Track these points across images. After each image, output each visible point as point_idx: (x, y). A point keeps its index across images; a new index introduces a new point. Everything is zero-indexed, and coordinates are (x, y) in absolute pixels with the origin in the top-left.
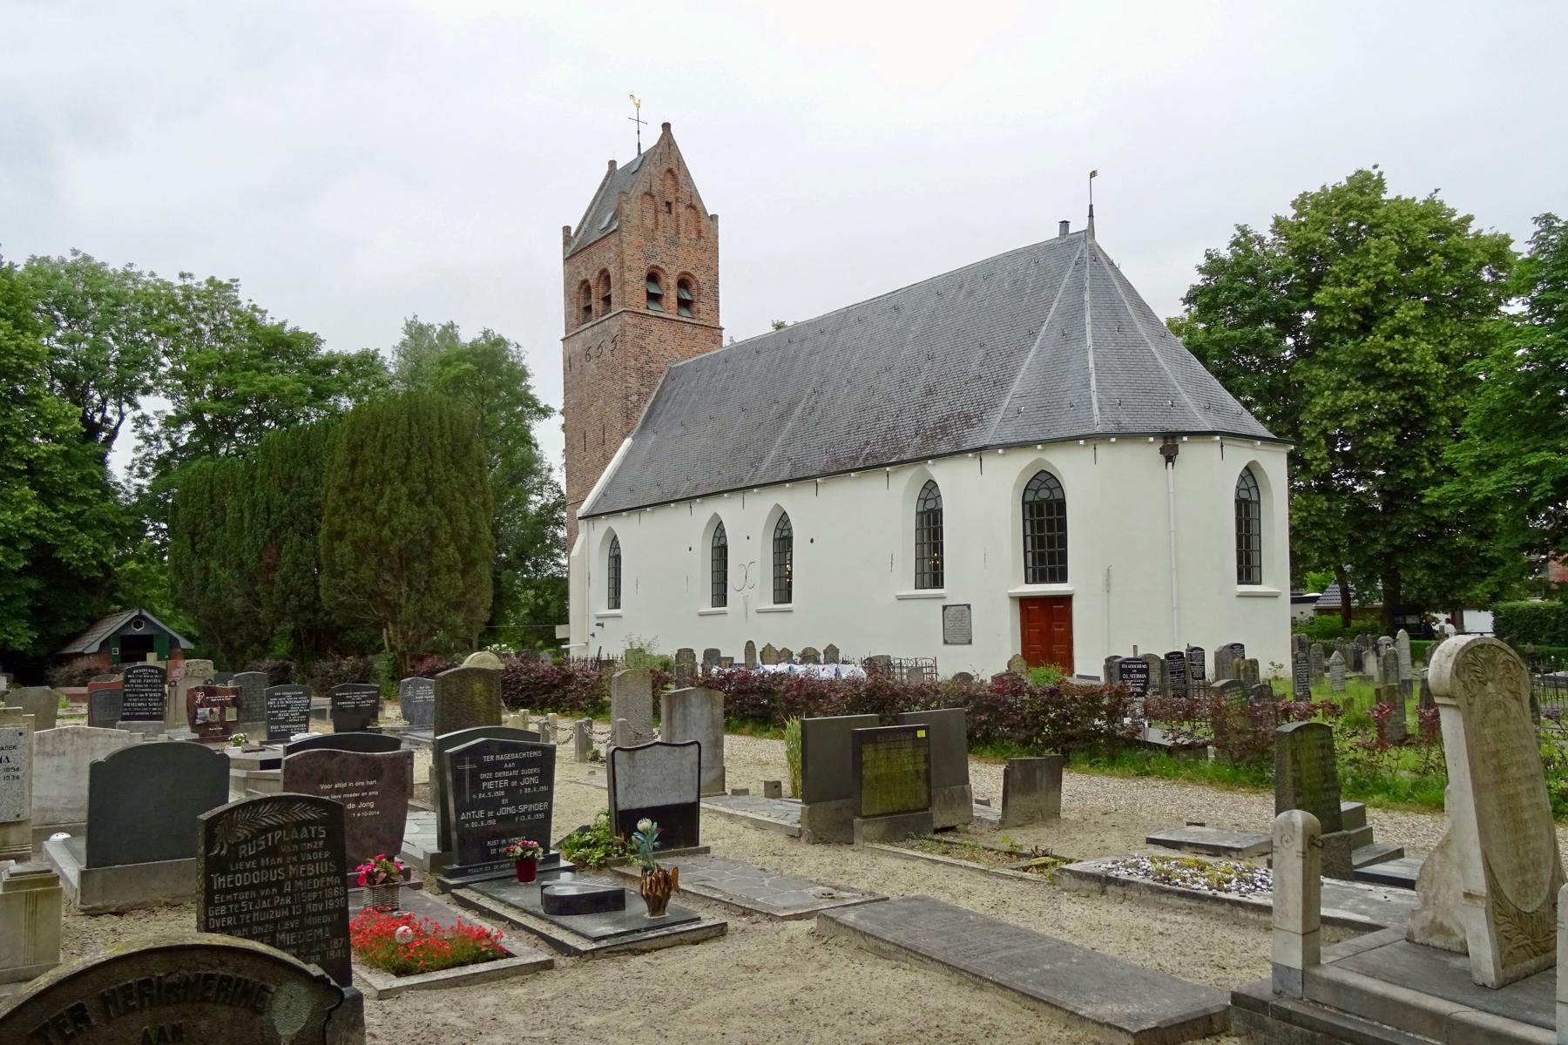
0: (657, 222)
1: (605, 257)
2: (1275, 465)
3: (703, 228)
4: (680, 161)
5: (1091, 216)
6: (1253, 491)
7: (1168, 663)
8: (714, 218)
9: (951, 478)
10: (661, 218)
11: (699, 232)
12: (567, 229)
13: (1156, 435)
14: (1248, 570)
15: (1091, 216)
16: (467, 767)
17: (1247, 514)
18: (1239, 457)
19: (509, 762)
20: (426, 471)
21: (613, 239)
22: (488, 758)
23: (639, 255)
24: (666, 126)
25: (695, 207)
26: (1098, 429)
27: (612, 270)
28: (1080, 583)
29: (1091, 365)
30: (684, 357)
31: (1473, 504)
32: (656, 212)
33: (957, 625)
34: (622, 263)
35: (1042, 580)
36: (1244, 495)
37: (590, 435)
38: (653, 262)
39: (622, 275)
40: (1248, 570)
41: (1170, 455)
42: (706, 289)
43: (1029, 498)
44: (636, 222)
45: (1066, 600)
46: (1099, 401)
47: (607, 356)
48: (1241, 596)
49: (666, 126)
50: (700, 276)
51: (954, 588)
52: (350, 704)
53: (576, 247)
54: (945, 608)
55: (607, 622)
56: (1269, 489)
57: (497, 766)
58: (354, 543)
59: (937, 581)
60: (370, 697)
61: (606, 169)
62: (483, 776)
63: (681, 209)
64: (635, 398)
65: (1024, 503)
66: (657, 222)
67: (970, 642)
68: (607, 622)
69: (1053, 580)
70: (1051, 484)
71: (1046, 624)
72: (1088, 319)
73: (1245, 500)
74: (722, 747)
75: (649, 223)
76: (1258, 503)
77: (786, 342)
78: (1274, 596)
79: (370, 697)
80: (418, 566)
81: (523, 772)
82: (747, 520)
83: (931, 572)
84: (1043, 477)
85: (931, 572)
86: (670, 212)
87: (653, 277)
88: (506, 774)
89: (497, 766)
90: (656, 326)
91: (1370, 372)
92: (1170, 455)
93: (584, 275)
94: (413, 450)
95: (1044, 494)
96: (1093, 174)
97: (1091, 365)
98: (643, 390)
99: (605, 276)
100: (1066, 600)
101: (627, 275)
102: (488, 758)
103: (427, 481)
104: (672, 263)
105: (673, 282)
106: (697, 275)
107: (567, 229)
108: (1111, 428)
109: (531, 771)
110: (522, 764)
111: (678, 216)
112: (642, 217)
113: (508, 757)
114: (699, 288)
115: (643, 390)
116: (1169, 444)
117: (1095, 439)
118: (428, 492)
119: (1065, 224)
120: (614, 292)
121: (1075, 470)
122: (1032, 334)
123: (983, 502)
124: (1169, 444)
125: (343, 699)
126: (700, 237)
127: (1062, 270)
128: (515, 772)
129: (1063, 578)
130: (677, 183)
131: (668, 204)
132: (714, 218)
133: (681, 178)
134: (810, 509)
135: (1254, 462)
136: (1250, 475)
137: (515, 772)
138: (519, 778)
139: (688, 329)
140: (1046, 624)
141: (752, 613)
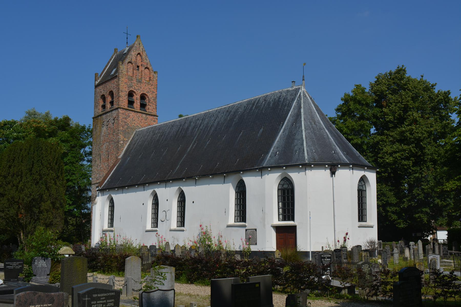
2: (372, 177)
6: (364, 186)
7: (335, 253)
9: (250, 181)
10: (135, 72)
11: (150, 78)
14: (362, 216)
16: (87, 299)
17: (362, 195)
18: (359, 174)
19: (102, 297)
20: (40, 171)
22: (95, 296)
23: (126, 86)
24: (436, 84)
27: (114, 91)
29: (304, 137)
30: (142, 127)
33: (251, 237)
34: (119, 89)
36: (361, 188)
39: (118, 93)
40: (362, 216)
41: (333, 173)
45: (294, 228)
46: (307, 150)
47: (111, 125)
52: (12, 267)
54: (246, 230)
57: (99, 299)
58: (8, 199)
59: (244, 220)
60: (20, 264)
62: (92, 303)
66: (133, 73)
67: (256, 244)
69: (289, 220)
71: (286, 235)
72: (303, 119)
74: (104, 272)
75: (130, 73)
76: (366, 191)
79: (20, 264)
80: (333, 271)
81: (108, 301)
82: (168, 194)
83: (242, 214)
85: (242, 214)
86: (138, 70)
87: (131, 94)
88: (101, 302)
89: (99, 299)
90: (132, 114)
91: (403, 140)
92: (333, 173)
93: (103, 93)
94: (35, 162)
98: (125, 139)
99: (111, 93)
101: (120, 94)
102: (95, 296)
103: (40, 175)
104: (139, 90)
105: (139, 97)
106: (148, 94)
109: (111, 301)
110: (107, 298)
112: (127, 71)
113: (102, 295)
115: (125, 139)
118: (40, 179)
125: (9, 265)
126: (150, 80)
127: (293, 100)
128: (105, 301)
129: (293, 220)
130: (142, 59)
131: (138, 67)
136: (363, 180)
137: (105, 301)
138: (106, 304)
139: (144, 116)
140: (286, 235)
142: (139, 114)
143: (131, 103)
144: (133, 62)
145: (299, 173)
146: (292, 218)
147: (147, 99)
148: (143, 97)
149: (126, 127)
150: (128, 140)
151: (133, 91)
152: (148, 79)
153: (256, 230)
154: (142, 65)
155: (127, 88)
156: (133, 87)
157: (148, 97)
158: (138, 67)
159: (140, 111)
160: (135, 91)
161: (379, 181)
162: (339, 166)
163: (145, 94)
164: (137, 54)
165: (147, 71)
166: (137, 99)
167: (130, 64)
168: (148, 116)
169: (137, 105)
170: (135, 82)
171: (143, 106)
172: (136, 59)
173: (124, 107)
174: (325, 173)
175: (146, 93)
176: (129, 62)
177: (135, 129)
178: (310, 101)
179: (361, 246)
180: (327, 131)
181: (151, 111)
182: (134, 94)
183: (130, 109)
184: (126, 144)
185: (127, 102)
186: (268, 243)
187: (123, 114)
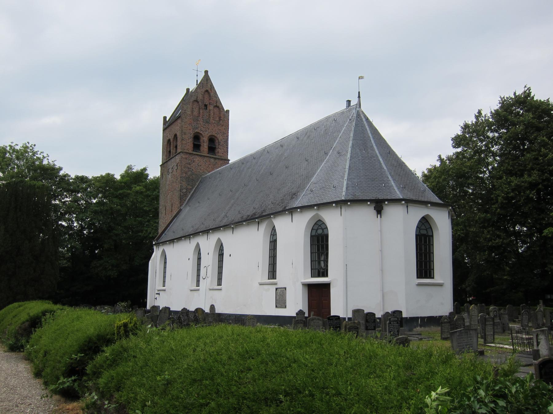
0: (199, 113)
1: (176, 129)
3: (222, 117)
4: (212, 87)
5: (359, 97)
6: (429, 230)
8: (228, 111)
9: (282, 224)
10: (201, 111)
11: (220, 117)
12: (165, 118)
13: (371, 201)
14: (425, 268)
15: (359, 97)
18: (417, 214)
21: (179, 121)
24: (206, 72)
25: (218, 106)
26: (343, 198)
27: (178, 134)
28: (334, 276)
31: (22, 181)
32: (199, 109)
35: (319, 276)
37: (167, 208)
38: (196, 131)
41: (379, 211)
42: (222, 143)
43: (314, 234)
44: (189, 113)
45: (327, 286)
47: (175, 173)
48: (419, 285)
49: (206, 72)
50: (220, 137)
51: (282, 279)
53: (168, 124)
54: (276, 289)
55: (161, 293)
56: (438, 229)
61: (185, 92)
63: (211, 107)
64: (185, 191)
65: (312, 236)
67: (286, 307)
68: (161, 293)
69: (426, 277)
70: (323, 227)
71: (318, 294)
73: (424, 235)
75: (196, 113)
77: (243, 162)
78: (441, 285)
82: (208, 244)
84: (320, 223)
86: (206, 109)
87: (197, 137)
90: (197, 159)
92: (379, 211)
95: (320, 231)
96: (361, 78)
97: (347, 167)
100: (327, 286)
104: (206, 131)
106: (218, 136)
107: (165, 118)
108: (350, 197)
111: (210, 110)
114: (219, 142)
116: (379, 206)
117: (341, 203)
119: (349, 102)
120: (179, 143)
121: (334, 220)
122: (326, 154)
123: (293, 232)
124: (379, 206)
126: (220, 120)
127: (345, 122)
130: (210, 96)
131: (206, 106)
132: (228, 111)
133: (212, 94)
134: (229, 239)
135: (428, 215)
139: (212, 160)
140: (318, 294)
141: (164, 288)
142: (206, 159)
143: (197, 147)
144: (199, 100)
145: (113, 175)
146: (324, 273)
147: (217, 141)
148: (212, 140)
149: (189, 173)
150: (192, 188)
151: (198, 133)
152: (217, 119)
153: (285, 288)
154: (210, 104)
155: (192, 130)
156: (199, 129)
157: (218, 139)
158: (206, 106)
159: (208, 155)
160: (201, 132)
161: (455, 224)
162: (386, 203)
163: (214, 136)
164: (203, 91)
165: (216, 110)
166: (204, 142)
167: (196, 103)
168: (217, 161)
169: (205, 146)
170: (202, 123)
171: (212, 149)
172: (204, 97)
173: (187, 151)
174: (368, 212)
175: (216, 135)
176: (195, 101)
177: (201, 176)
178: (365, 122)
179: (401, 312)
180: (381, 160)
181: (221, 155)
182: (201, 136)
183: (194, 153)
184: (190, 192)
185: (192, 145)
186: (296, 304)
187: (186, 158)
